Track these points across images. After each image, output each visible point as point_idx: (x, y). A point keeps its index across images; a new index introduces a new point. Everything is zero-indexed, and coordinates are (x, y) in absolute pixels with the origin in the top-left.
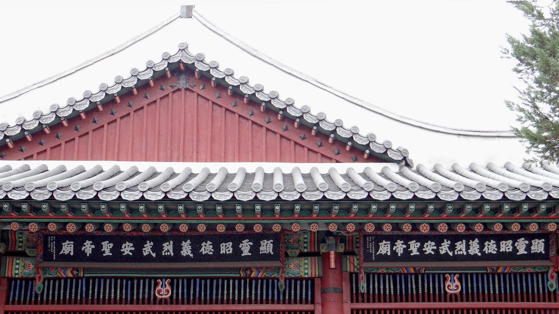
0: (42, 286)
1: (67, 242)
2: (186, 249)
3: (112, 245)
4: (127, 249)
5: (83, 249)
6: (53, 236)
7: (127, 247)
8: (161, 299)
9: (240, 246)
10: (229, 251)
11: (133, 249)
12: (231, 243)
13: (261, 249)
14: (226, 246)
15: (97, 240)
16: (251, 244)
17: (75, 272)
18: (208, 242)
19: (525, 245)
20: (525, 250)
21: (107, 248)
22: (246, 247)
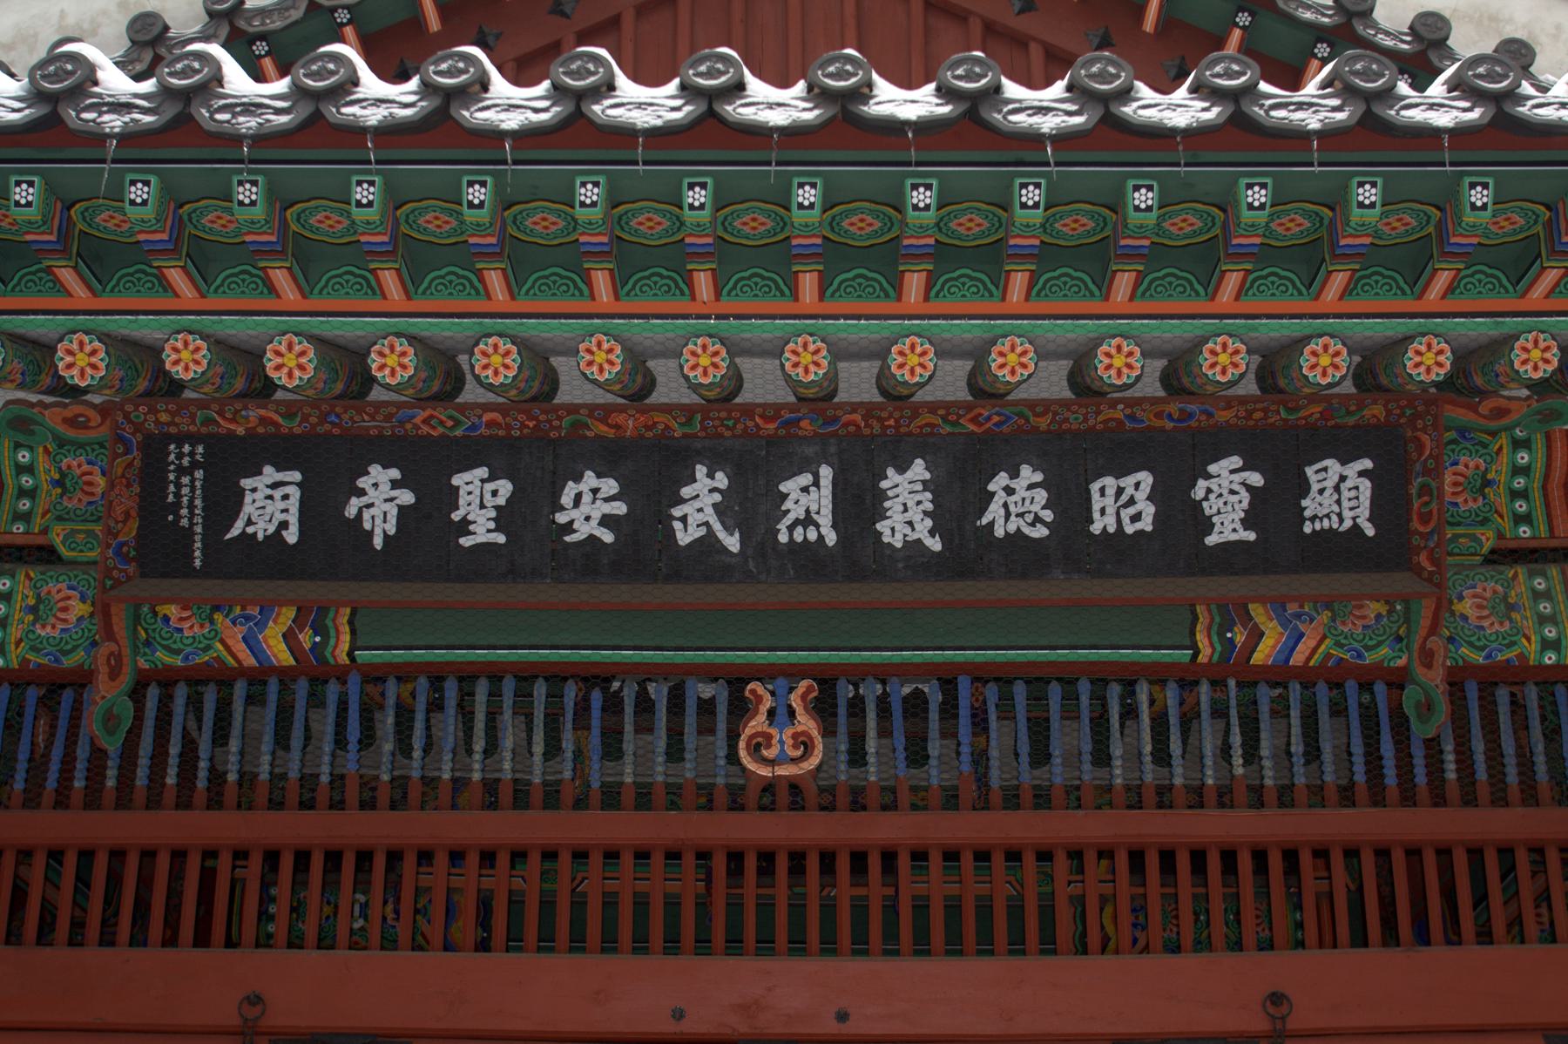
0: (127, 710)
1: (270, 474)
2: (907, 509)
3: (505, 487)
4: (589, 507)
5: (351, 511)
6: (194, 439)
7: (587, 498)
8: (769, 787)
9: (1199, 492)
10: (1136, 518)
11: (620, 508)
12: (1146, 478)
13: (1309, 505)
14: (1120, 491)
15: (430, 469)
16: (1256, 479)
17: (307, 639)
18: (1026, 470)
19: (1245, 496)
20: (1247, 523)
21: (479, 499)
22: (479, 499)
